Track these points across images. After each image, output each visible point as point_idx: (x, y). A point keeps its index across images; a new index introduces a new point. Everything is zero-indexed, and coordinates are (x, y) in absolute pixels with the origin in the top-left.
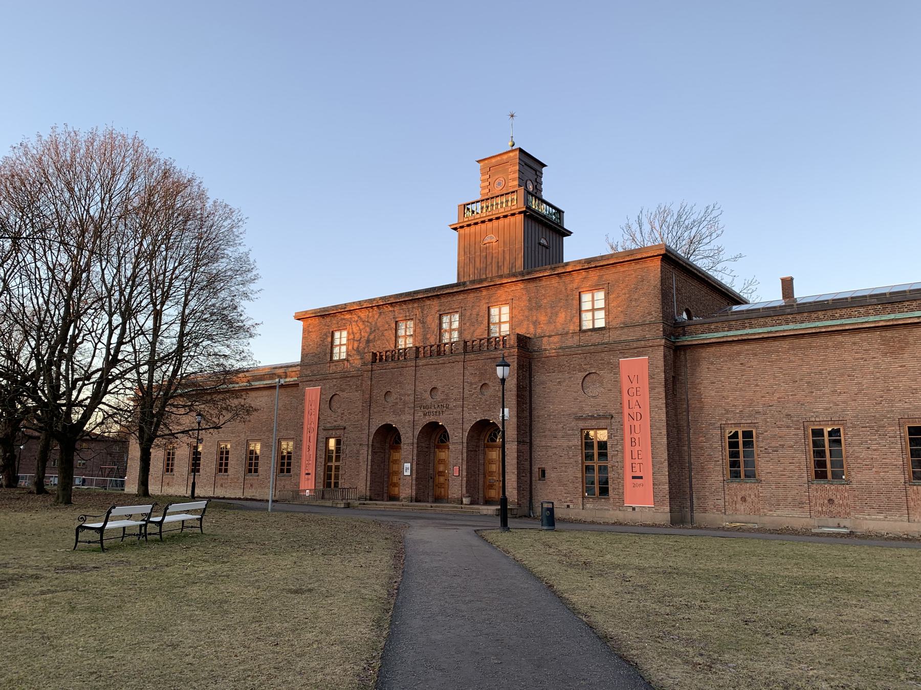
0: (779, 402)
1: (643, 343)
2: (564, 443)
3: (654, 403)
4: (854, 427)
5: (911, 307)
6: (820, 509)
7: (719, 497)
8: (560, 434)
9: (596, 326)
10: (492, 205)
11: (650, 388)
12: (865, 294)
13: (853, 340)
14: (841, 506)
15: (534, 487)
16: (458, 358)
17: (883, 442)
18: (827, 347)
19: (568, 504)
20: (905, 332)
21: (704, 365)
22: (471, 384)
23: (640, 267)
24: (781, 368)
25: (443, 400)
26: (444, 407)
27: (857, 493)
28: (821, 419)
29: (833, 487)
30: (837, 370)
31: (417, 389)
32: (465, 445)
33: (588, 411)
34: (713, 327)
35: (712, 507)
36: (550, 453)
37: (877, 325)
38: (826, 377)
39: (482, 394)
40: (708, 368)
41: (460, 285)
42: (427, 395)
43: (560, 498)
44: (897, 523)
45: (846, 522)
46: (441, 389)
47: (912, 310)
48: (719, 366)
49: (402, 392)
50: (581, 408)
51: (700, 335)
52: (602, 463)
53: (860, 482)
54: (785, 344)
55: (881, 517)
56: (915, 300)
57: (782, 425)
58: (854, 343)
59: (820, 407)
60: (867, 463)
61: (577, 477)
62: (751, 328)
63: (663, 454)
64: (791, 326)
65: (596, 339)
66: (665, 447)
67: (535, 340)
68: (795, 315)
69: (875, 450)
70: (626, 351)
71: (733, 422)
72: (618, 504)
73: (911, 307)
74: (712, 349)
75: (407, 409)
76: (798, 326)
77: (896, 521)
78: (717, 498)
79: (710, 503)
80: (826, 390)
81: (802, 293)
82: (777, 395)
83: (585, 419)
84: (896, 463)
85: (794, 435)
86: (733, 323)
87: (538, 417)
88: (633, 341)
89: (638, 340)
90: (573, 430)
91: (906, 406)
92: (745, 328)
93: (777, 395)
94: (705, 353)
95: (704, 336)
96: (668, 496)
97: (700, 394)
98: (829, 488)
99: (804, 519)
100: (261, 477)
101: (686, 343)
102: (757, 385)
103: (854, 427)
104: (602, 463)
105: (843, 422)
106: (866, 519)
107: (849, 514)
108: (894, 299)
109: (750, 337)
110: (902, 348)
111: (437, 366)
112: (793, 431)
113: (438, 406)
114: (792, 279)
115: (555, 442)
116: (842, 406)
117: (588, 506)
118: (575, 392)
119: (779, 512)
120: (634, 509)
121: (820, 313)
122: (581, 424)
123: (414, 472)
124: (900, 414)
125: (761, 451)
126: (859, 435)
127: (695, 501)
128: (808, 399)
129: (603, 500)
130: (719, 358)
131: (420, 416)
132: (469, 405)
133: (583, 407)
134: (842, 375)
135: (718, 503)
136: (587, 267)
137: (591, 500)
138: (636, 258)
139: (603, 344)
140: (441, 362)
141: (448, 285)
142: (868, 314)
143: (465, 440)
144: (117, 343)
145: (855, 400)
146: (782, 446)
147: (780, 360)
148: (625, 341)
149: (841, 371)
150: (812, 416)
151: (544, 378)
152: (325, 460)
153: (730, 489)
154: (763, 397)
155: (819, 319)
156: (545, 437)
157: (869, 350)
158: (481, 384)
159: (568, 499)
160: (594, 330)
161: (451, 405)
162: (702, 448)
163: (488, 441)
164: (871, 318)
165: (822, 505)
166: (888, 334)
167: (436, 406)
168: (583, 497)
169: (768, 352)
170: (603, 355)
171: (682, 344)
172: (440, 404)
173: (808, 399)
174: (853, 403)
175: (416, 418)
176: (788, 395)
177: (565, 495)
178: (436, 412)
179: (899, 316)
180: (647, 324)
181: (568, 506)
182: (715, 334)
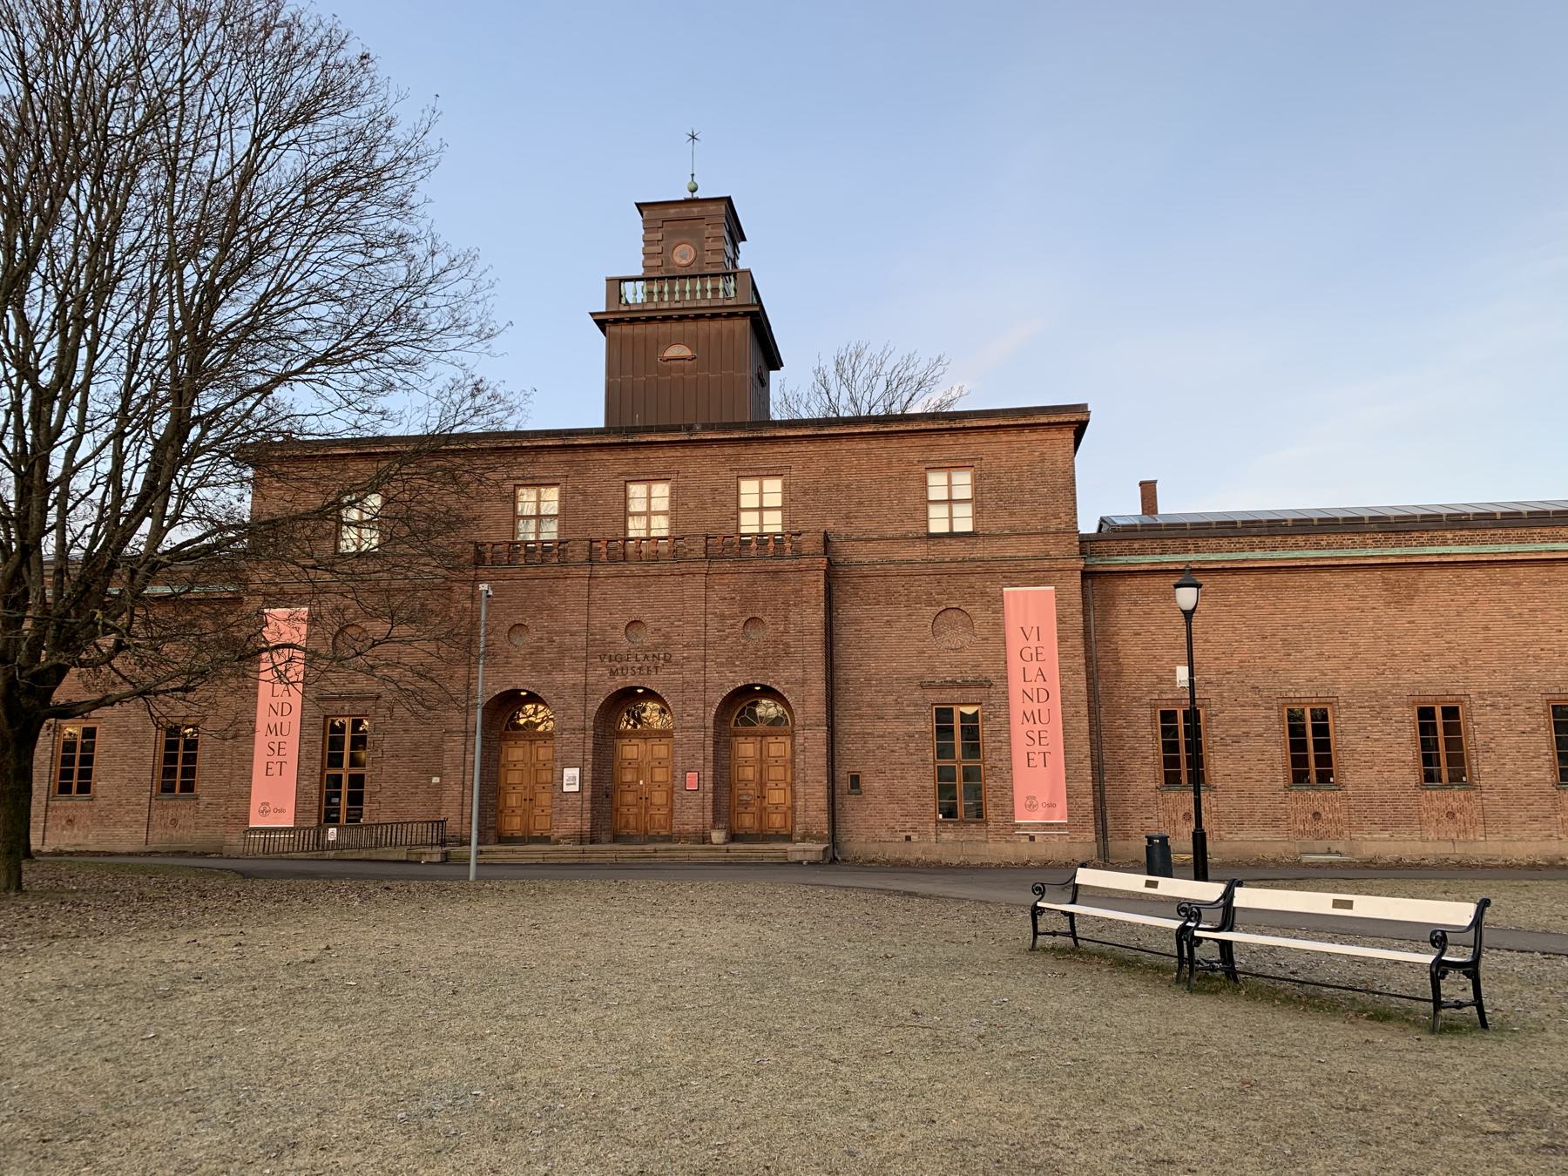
0: (1241, 667)
1: (1046, 563)
2: (901, 728)
3: (1068, 663)
4: (1349, 706)
5: (1422, 540)
6: (1302, 827)
7: (1150, 815)
8: (891, 712)
9: (956, 529)
10: (661, 292)
11: (1059, 638)
12: (1262, 518)
13: (1345, 580)
14: (1330, 822)
15: (838, 806)
16: (693, 567)
17: (1387, 729)
18: (1310, 589)
19: (909, 834)
20: (1413, 574)
21: (1123, 606)
22: (723, 617)
23: (1039, 437)
24: (1243, 617)
25: (656, 646)
26: (661, 657)
27: (1353, 802)
28: (1303, 694)
29: (1319, 795)
30: (1324, 624)
31: (595, 622)
32: (710, 732)
33: (945, 673)
34: (1136, 546)
35: (1139, 830)
36: (871, 746)
37: (1385, 561)
38: (1309, 633)
39: (746, 636)
40: (1129, 611)
41: (680, 431)
42: (619, 635)
43: (891, 825)
44: (1407, 843)
45: (1340, 846)
46: (651, 624)
47: (1422, 544)
48: (1146, 609)
49: (556, 626)
50: (932, 669)
51: (1116, 558)
52: (970, 763)
53: (1357, 787)
54: (1249, 581)
55: (1386, 835)
56: (1427, 531)
57: (1246, 702)
58: (1347, 586)
59: (1301, 677)
60: (1366, 759)
61: (925, 787)
62: (1197, 552)
63: (1082, 746)
64: (1258, 554)
65: (957, 549)
66: (1086, 734)
67: (838, 545)
68: (1263, 539)
69: (1376, 740)
70: (1013, 575)
71: (1170, 696)
72: (1002, 831)
73: (1422, 540)
74: (1137, 581)
75: (567, 661)
76: (1269, 555)
77: (1404, 840)
78: (1147, 816)
79: (1136, 824)
80: (1308, 653)
81: (1171, 506)
82: (1237, 657)
83: (942, 687)
84: (1403, 759)
85: (1264, 717)
86: (1169, 542)
87: (847, 682)
88: (1027, 559)
89: (1035, 558)
90: (916, 705)
91: (1417, 678)
92: (1187, 551)
93: (1237, 657)
94: (1124, 586)
95: (1123, 559)
96: (1092, 816)
97: (1116, 651)
98: (1315, 797)
99: (1279, 844)
100: (101, 802)
101: (1100, 569)
102: (1207, 641)
103: (1349, 706)
104: (970, 763)
105: (1333, 701)
106: (1366, 840)
107: (1341, 833)
108: (1400, 527)
109: (1203, 566)
110: (1410, 597)
111: (642, 579)
112: (1262, 712)
113: (646, 657)
114: (1155, 482)
115: (880, 727)
116: (1331, 675)
117: (945, 836)
118: (919, 640)
119: (1242, 835)
120: (1032, 838)
121: (1299, 538)
122: (933, 696)
123: (587, 785)
124: (1409, 688)
125: (1214, 742)
126: (1355, 719)
127: (1110, 821)
128: (1283, 665)
129: (973, 826)
130: (1146, 595)
131: (601, 675)
132: (717, 656)
133: (935, 667)
134: (1331, 631)
135: (1148, 824)
136: (948, 426)
137: (950, 826)
138: (1038, 421)
139: (973, 560)
140: (652, 572)
141: (592, 429)
142: (1365, 546)
143: (710, 722)
144: (56, 480)
145: (1349, 668)
146: (1247, 734)
147: (1241, 604)
148: (1012, 558)
149: (1328, 625)
150: (1290, 690)
151: (857, 612)
152: (322, 764)
153: (1165, 801)
154: (1217, 659)
155: (1297, 547)
156: (861, 717)
157: (1367, 597)
158: (744, 619)
159: (908, 825)
160: (952, 535)
161: (677, 657)
162: (1120, 737)
163: (736, 725)
164: (1370, 552)
165: (1304, 822)
166: (1392, 575)
167: (641, 657)
168: (937, 821)
169: (1224, 592)
170: (972, 579)
171: (1093, 569)
172: (650, 654)
173: (1283, 665)
174: (1346, 672)
175: (592, 679)
176: (1254, 658)
177: (902, 819)
178: (640, 668)
179: (1406, 551)
180: (1053, 533)
181: (908, 838)
182: (1140, 557)
